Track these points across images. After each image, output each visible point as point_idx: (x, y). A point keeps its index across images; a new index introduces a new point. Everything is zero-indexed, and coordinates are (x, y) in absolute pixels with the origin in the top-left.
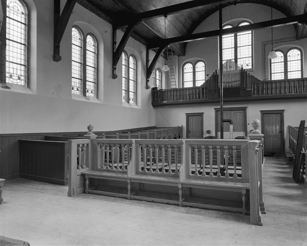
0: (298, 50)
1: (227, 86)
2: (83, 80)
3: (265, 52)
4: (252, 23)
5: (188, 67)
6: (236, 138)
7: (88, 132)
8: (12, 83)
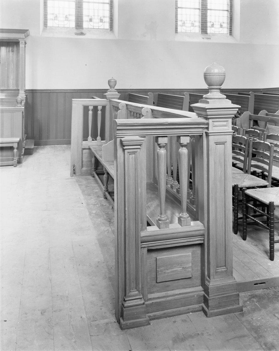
2: (202, 9)
6: (145, 137)
7: (109, 89)
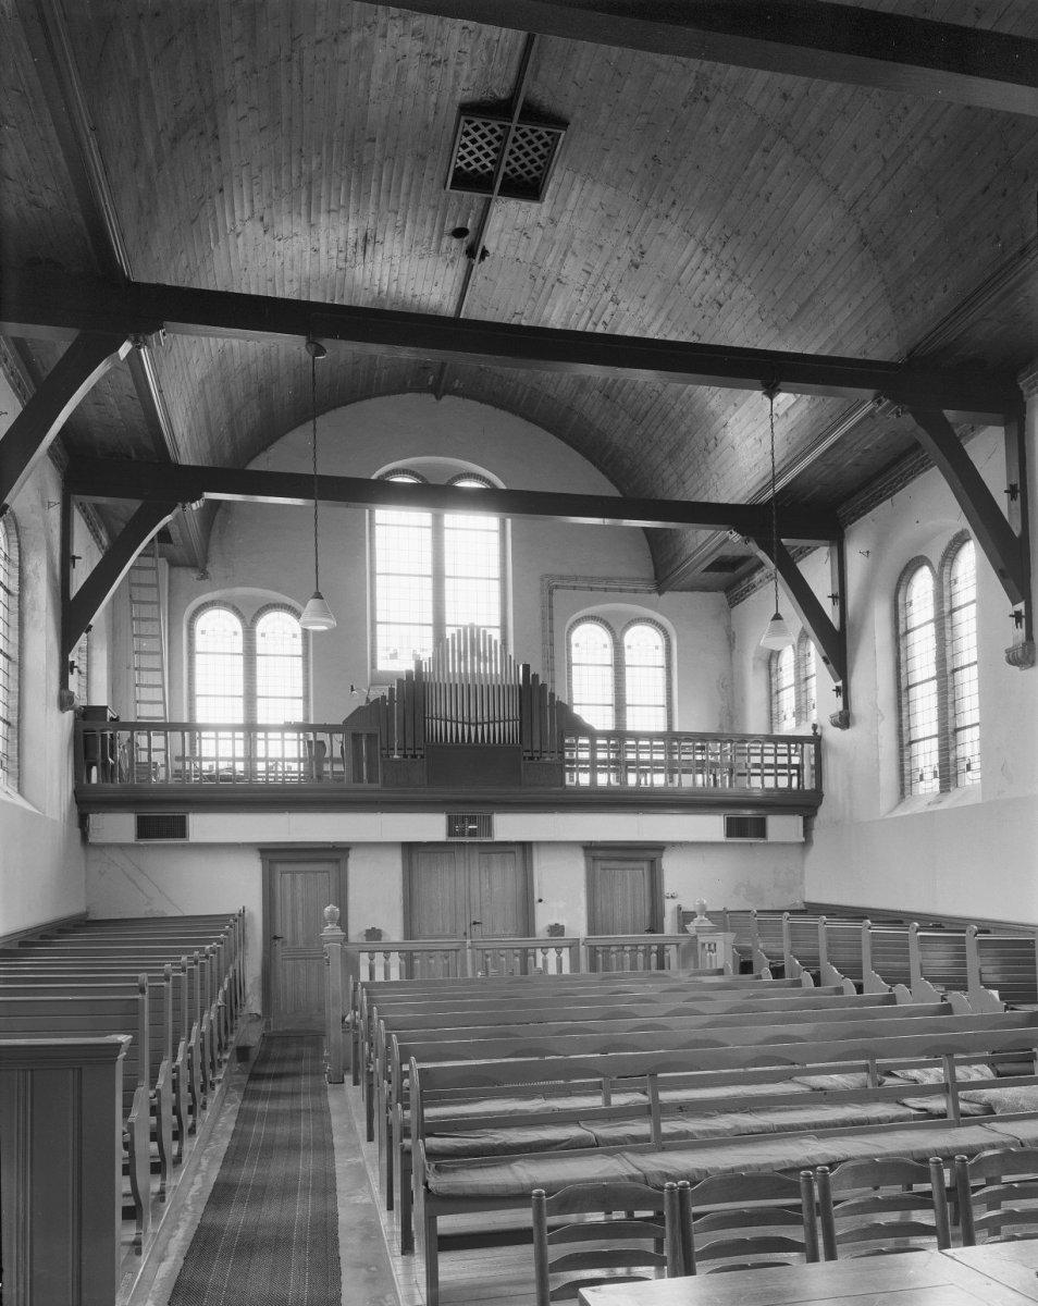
1: (469, 737)
3: (551, 618)
4: (502, 486)
5: (217, 629)
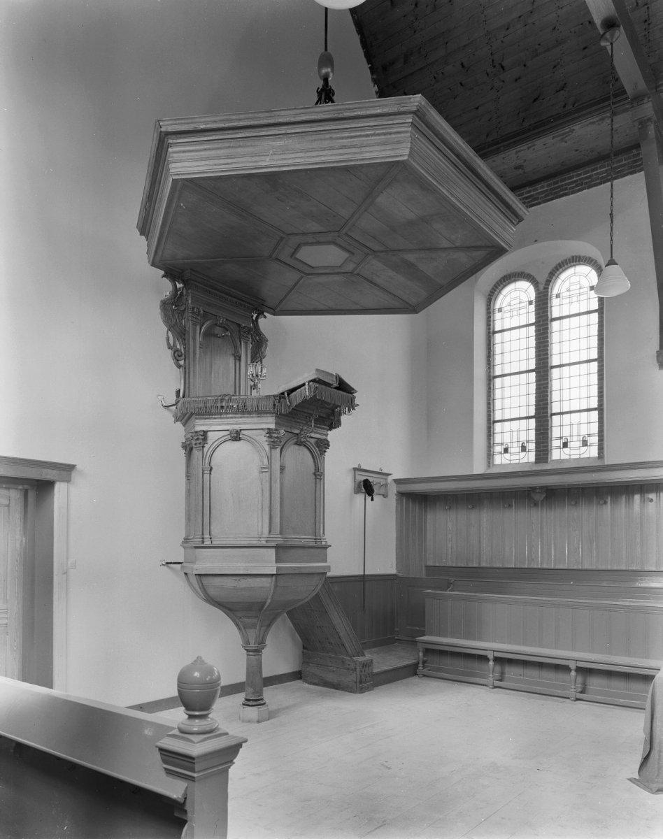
0: (590, 268)
8: (568, 457)
